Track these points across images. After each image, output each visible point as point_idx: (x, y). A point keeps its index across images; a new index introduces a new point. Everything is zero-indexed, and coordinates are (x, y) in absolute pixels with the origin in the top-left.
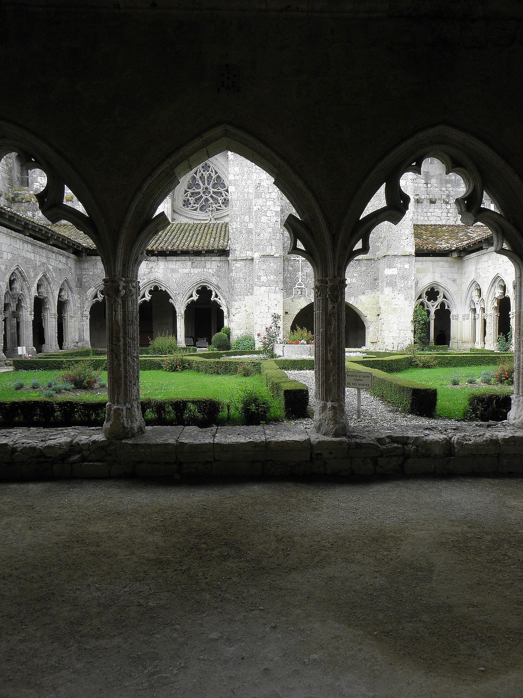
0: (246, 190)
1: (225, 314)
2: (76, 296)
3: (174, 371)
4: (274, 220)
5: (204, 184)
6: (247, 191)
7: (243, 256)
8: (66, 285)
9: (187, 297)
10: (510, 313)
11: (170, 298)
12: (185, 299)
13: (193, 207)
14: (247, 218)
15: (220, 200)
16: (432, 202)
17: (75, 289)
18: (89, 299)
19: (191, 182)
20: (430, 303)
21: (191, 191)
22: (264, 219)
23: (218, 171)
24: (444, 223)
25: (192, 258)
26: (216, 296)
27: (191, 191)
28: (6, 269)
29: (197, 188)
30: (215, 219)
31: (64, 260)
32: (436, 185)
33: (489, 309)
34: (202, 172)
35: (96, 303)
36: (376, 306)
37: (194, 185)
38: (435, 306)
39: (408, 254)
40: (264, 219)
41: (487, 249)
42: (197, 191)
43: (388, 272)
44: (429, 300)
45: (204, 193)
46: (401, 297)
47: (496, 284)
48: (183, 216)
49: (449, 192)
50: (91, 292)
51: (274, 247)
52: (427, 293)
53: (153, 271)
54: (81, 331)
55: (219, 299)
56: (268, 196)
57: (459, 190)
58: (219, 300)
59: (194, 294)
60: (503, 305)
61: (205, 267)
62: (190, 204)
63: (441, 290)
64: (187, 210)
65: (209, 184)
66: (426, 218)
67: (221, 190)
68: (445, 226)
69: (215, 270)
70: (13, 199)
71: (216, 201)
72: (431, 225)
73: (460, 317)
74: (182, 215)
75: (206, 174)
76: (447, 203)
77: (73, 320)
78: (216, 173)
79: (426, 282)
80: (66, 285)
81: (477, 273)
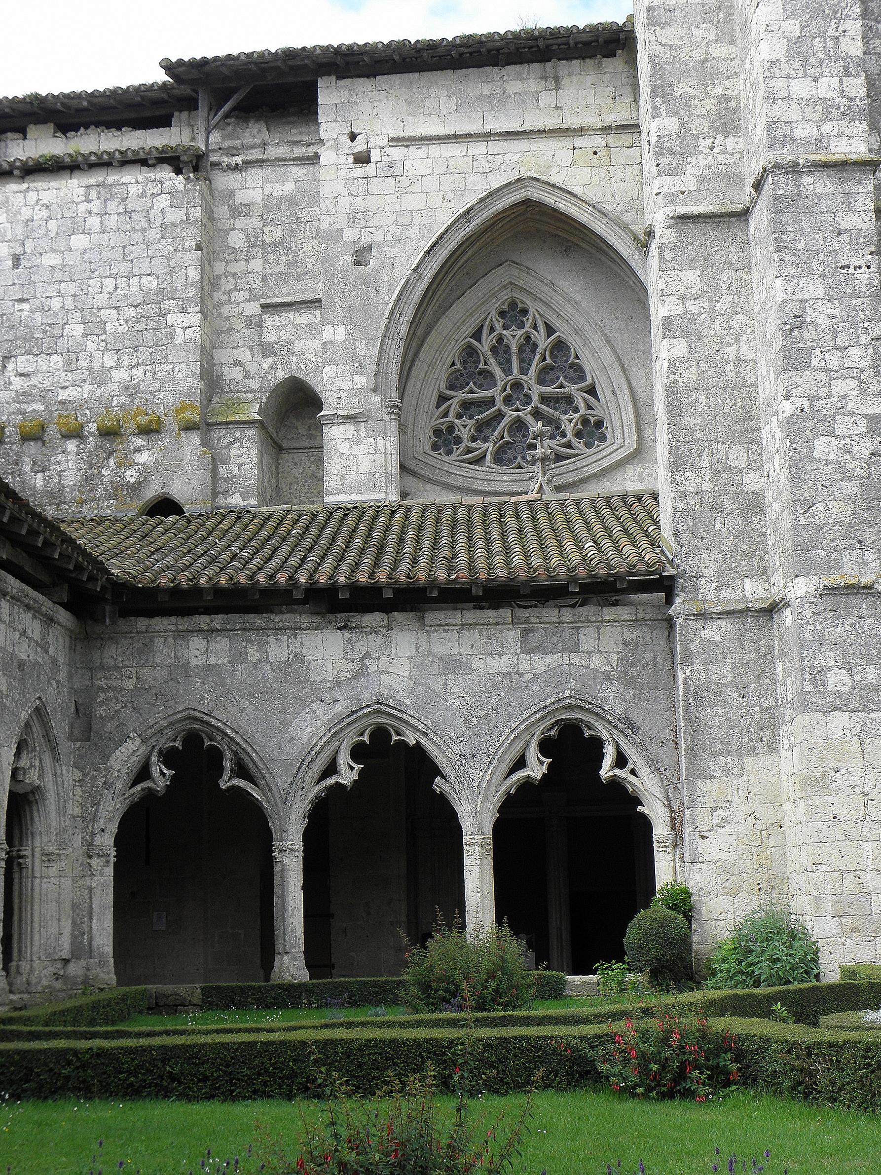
0: (730, 351)
1: (660, 830)
2: (70, 775)
3: (668, 1095)
5: (508, 371)
6: (732, 357)
7: (731, 597)
8: (36, 729)
9: (504, 768)
11: (437, 771)
12: (500, 776)
13: (469, 451)
14: (737, 457)
15: (569, 423)
17: (65, 746)
18: (119, 786)
19: (459, 365)
22: (822, 447)
23: (556, 323)
25: (523, 613)
26: (621, 761)
27: (461, 395)
29: (481, 387)
30: (558, 489)
31: (34, 628)
34: (499, 329)
35: (142, 799)
37: (471, 375)
40: (822, 447)
42: (482, 394)
45: (508, 400)
50: (126, 755)
53: (372, 668)
54: (82, 913)
55: (633, 772)
58: (631, 778)
59: (533, 754)
61: (575, 648)
62: (458, 440)
63: (222, 746)
64: (450, 465)
65: (524, 370)
67: (571, 389)
69: (614, 658)
71: (557, 430)
74: (429, 480)
75: (514, 338)
77: (53, 871)
78: (550, 330)
80: (36, 729)
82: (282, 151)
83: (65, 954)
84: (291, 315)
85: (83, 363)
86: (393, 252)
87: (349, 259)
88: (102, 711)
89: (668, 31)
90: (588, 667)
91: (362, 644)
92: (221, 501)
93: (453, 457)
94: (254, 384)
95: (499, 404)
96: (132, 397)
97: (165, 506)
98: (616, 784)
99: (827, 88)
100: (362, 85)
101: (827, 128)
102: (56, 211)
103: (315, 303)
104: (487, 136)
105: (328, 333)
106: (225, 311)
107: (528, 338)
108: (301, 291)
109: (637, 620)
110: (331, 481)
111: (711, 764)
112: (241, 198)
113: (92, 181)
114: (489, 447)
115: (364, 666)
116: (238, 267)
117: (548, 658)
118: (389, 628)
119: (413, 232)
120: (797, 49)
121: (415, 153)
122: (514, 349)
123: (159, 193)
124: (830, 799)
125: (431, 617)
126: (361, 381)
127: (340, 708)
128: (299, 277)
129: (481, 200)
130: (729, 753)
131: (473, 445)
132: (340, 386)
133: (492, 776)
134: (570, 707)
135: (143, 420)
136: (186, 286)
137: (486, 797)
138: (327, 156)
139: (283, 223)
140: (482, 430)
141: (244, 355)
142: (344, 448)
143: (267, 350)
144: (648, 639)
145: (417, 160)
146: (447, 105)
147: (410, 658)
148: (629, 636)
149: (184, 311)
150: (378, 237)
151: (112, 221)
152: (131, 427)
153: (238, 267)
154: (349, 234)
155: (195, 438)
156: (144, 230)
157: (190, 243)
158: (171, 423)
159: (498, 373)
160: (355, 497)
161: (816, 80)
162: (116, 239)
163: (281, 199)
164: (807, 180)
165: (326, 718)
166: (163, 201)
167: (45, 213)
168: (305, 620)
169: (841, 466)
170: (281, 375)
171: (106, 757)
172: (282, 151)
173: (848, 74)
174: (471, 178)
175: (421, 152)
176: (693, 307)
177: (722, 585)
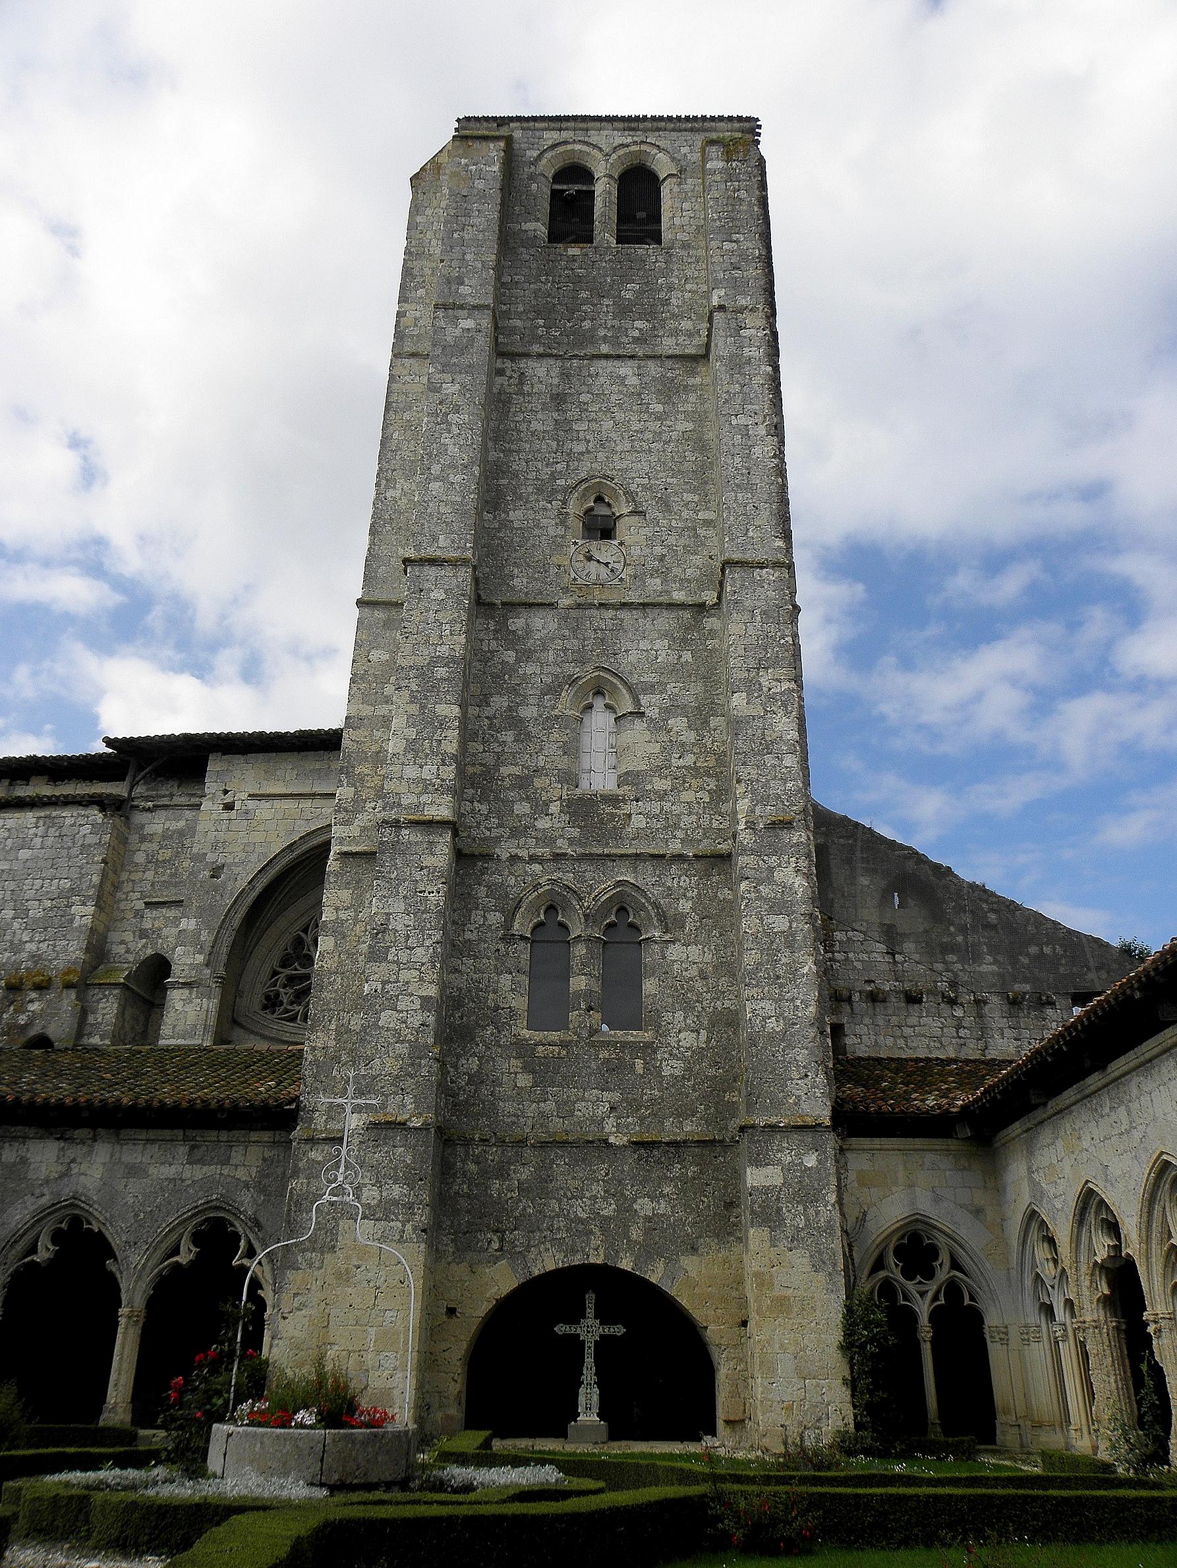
4: (415, 1021)
9: (159, 1253)
10: (1146, 1316)
13: (287, 1011)
16: (913, 999)
19: (290, 951)
20: (911, 1286)
21: (288, 972)
24: (953, 1056)
25: (191, 1133)
27: (288, 972)
32: (916, 957)
33: (1087, 1305)
36: (734, 1294)
37: (298, 958)
38: (930, 1295)
39: (810, 1121)
41: (1045, 1104)
42: (303, 971)
43: (755, 1177)
44: (908, 1275)
46: (800, 1260)
47: (1091, 1218)
48: (257, 1034)
49: (956, 975)
51: (408, 1100)
52: (899, 1252)
56: (404, 956)
57: (981, 969)
60: (1123, 1284)
61: (226, 1162)
62: (282, 1003)
63: (941, 1241)
66: (901, 1042)
68: (955, 1061)
72: (917, 1060)
73: (1014, 1333)
74: (252, 1032)
76: (952, 1002)
79: (889, 1213)
81: (1034, 1185)
82: (183, 800)
84: (164, 910)
85: (8, 938)
86: (236, 870)
87: (207, 873)
89: (358, 732)
90: (233, 1177)
91: (73, 1151)
92: (85, 1041)
93: (275, 1016)
94: (131, 958)
96: (36, 963)
97: (43, 1042)
99: (428, 772)
100: (239, 759)
101: (425, 798)
102: (14, 833)
103: (179, 903)
104: (313, 796)
105: (184, 924)
106: (122, 906)
108: (176, 894)
109: (274, 1142)
110: (166, 1030)
111: (299, 1258)
112: (148, 830)
113: (42, 814)
115: (69, 1169)
116: (136, 876)
117: (205, 1168)
118: (94, 1140)
119: (253, 858)
120: (412, 747)
121: (264, 804)
123: (86, 824)
124: (349, 1290)
125: (125, 1133)
126: (200, 958)
127: (45, 1200)
128: (176, 885)
129: (301, 838)
130: (314, 1250)
131: (290, 1007)
132: (186, 961)
133: (147, 1260)
134: (217, 1208)
135: (38, 979)
136: (89, 888)
137: (139, 1278)
138: (206, 805)
139: (172, 848)
141: (128, 937)
142: (179, 1006)
143: (143, 934)
144: (281, 1157)
145: (264, 810)
146: (291, 775)
147: (104, 1164)
148: (268, 1154)
149: (84, 904)
150: (230, 860)
151: (50, 841)
152: (29, 984)
153: (136, 876)
154: (210, 857)
155: (73, 994)
156: (69, 848)
157: (98, 858)
158: (57, 982)
160: (180, 1042)
161: (421, 767)
162: (48, 853)
163: (174, 832)
164: (405, 832)
165: (32, 1208)
166: (86, 829)
167: (6, 834)
168: (32, 1131)
170: (150, 952)
172: (183, 800)
173: (444, 764)
174: (299, 822)
175: (268, 805)
176: (343, 915)
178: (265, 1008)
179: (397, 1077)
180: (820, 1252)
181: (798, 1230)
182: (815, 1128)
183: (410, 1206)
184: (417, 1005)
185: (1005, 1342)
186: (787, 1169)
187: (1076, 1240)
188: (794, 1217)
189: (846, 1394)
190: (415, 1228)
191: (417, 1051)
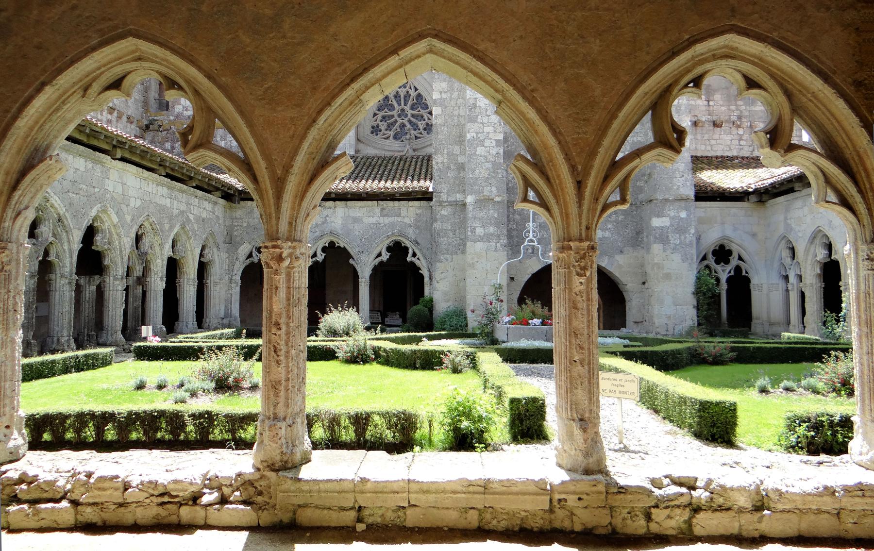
1: (426, 279)
2: (224, 256)
3: (66, 373)
4: (494, 151)
5: (399, 105)
11: (351, 257)
15: (421, 125)
16: (716, 125)
26: (414, 255)
27: (381, 114)
28: (133, 219)
29: (389, 110)
31: (209, 206)
32: (721, 103)
37: (386, 105)
38: (728, 271)
42: (390, 113)
43: (656, 222)
45: (399, 116)
46: (677, 257)
49: (741, 112)
51: (494, 189)
54: (228, 302)
56: (485, 120)
62: (380, 131)
64: (377, 139)
65: (406, 104)
67: (423, 112)
68: (737, 158)
70: (148, 127)
77: (218, 288)
83: (222, 316)
88: (236, 233)
95: (396, 117)
98: (412, 263)
107: (408, 92)
114: (392, 133)
117: (390, 219)
122: (402, 96)
140: (389, 127)
159: (396, 105)
169: (486, 157)
171: (237, 249)
176: (444, 96)
177: (449, 195)
178: (372, 133)
179: (488, 178)
180: (686, 255)
181: (676, 245)
182: (687, 199)
183: (498, 236)
184: (494, 144)
185: (760, 290)
186: (672, 218)
187: (807, 251)
188: (675, 239)
189: (694, 311)
190: (501, 245)
191: (495, 166)
